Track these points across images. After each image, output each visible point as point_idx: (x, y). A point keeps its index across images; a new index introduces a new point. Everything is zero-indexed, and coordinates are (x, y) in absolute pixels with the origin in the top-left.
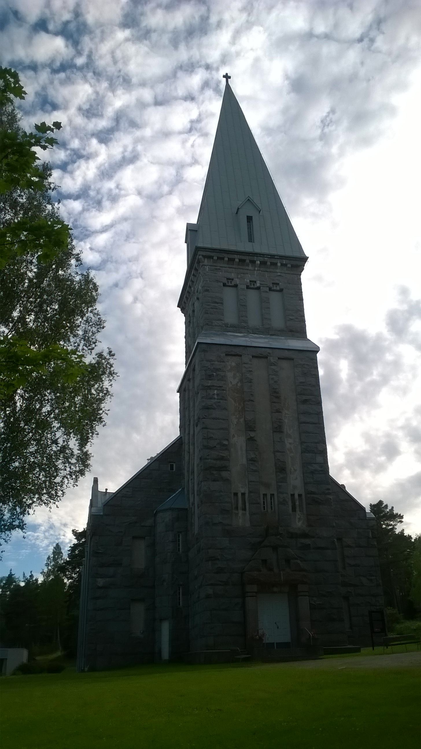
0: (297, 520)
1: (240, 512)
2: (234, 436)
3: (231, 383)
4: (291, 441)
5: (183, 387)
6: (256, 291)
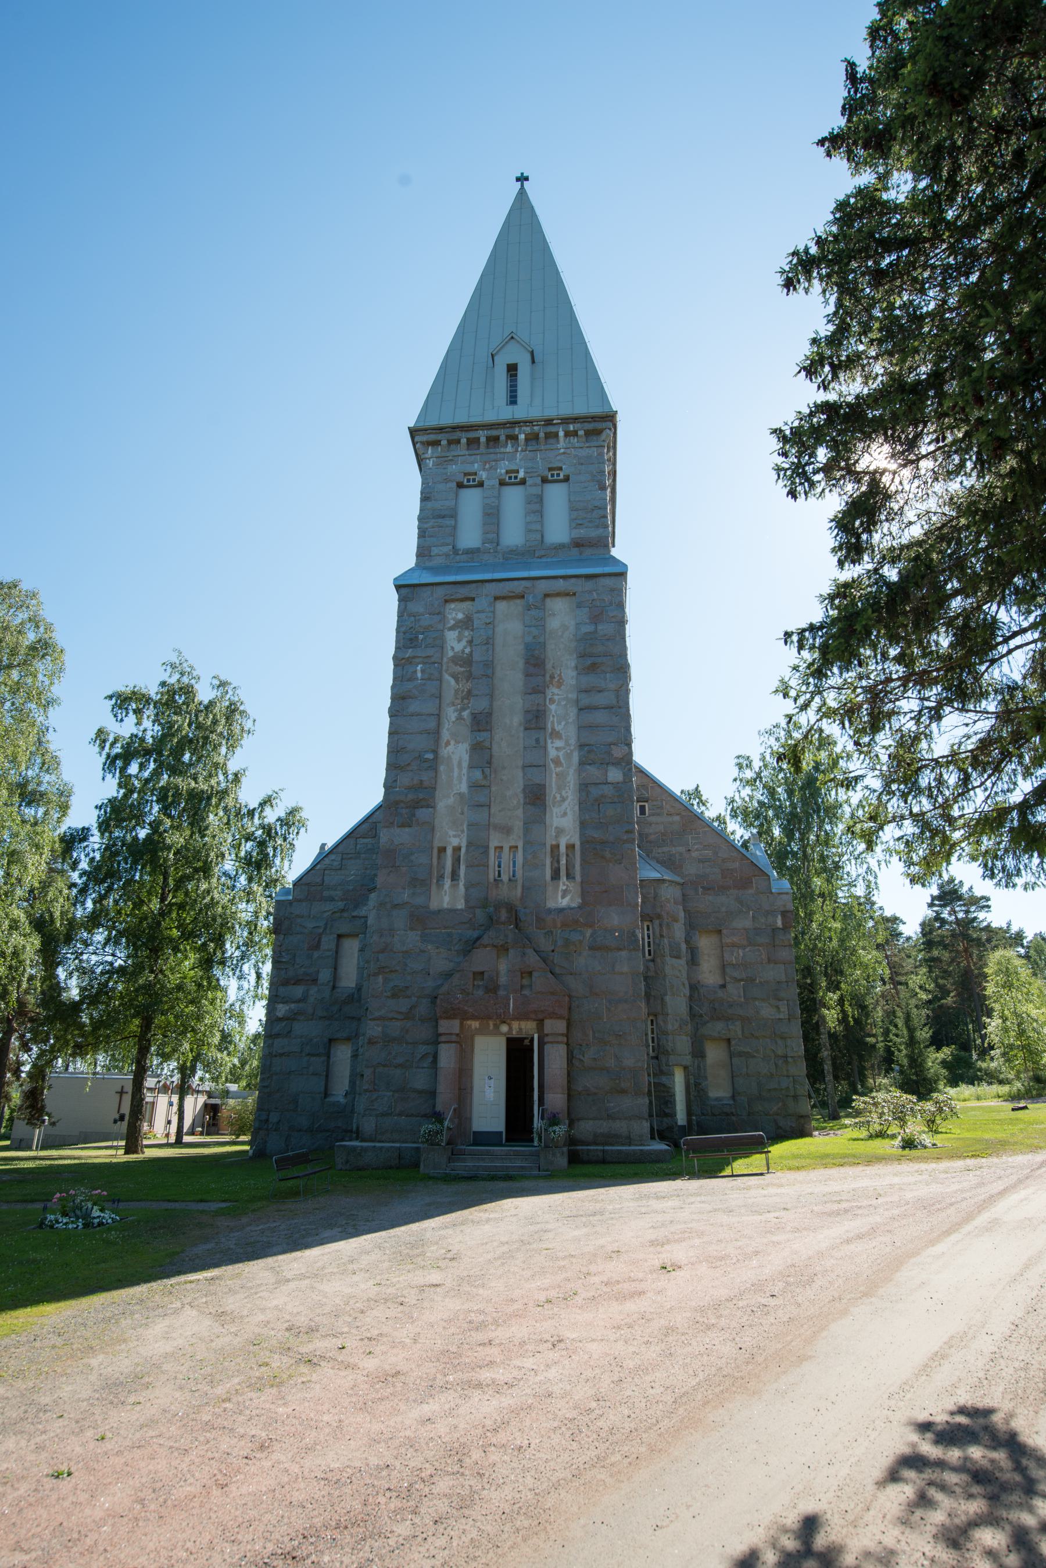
0: (560, 894)
1: (447, 883)
2: (448, 743)
3: (453, 648)
4: (559, 743)
5: (340, 849)
6: (519, 489)
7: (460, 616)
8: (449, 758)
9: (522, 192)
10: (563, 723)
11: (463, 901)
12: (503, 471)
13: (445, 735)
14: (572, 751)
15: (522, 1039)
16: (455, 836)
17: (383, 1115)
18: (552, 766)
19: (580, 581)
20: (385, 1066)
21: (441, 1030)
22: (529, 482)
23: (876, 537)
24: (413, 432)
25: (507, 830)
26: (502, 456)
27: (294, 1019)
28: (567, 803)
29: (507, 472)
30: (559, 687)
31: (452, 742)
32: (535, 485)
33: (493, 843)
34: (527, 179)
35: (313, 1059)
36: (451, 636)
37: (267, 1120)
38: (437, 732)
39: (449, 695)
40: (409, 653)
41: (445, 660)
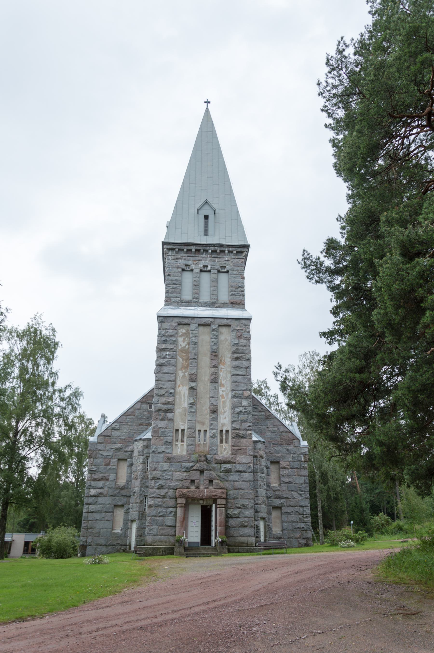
2: (179, 386)
3: (181, 345)
4: (223, 389)
7: (184, 331)
8: (180, 392)
9: (207, 111)
10: (225, 381)
11: (185, 451)
12: (202, 266)
13: (178, 382)
14: (228, 392)
15: (207, 506)
16: (182, 425)
17: (154, 535)
18: (221, 398)
19: (233, 321)
20: (155, 516)
21: (178, 502)
22: (213, 271)
23: (425, 79)
24: (164, 244)
25: (203, 424)
26: (201, 258)
27: (98, 496)
28: (226, 413)
29: (203, 266)
30: (223, 365)
31: (181, 386)
32: (214, 273)
33: (198, 428)
34: (209, 103)
35: (107, 514)
36: (180, 339)
37: (86, 541)
38: (175, 381)
39: (179, 366)
40: (164, 346)
41: (178, 350)
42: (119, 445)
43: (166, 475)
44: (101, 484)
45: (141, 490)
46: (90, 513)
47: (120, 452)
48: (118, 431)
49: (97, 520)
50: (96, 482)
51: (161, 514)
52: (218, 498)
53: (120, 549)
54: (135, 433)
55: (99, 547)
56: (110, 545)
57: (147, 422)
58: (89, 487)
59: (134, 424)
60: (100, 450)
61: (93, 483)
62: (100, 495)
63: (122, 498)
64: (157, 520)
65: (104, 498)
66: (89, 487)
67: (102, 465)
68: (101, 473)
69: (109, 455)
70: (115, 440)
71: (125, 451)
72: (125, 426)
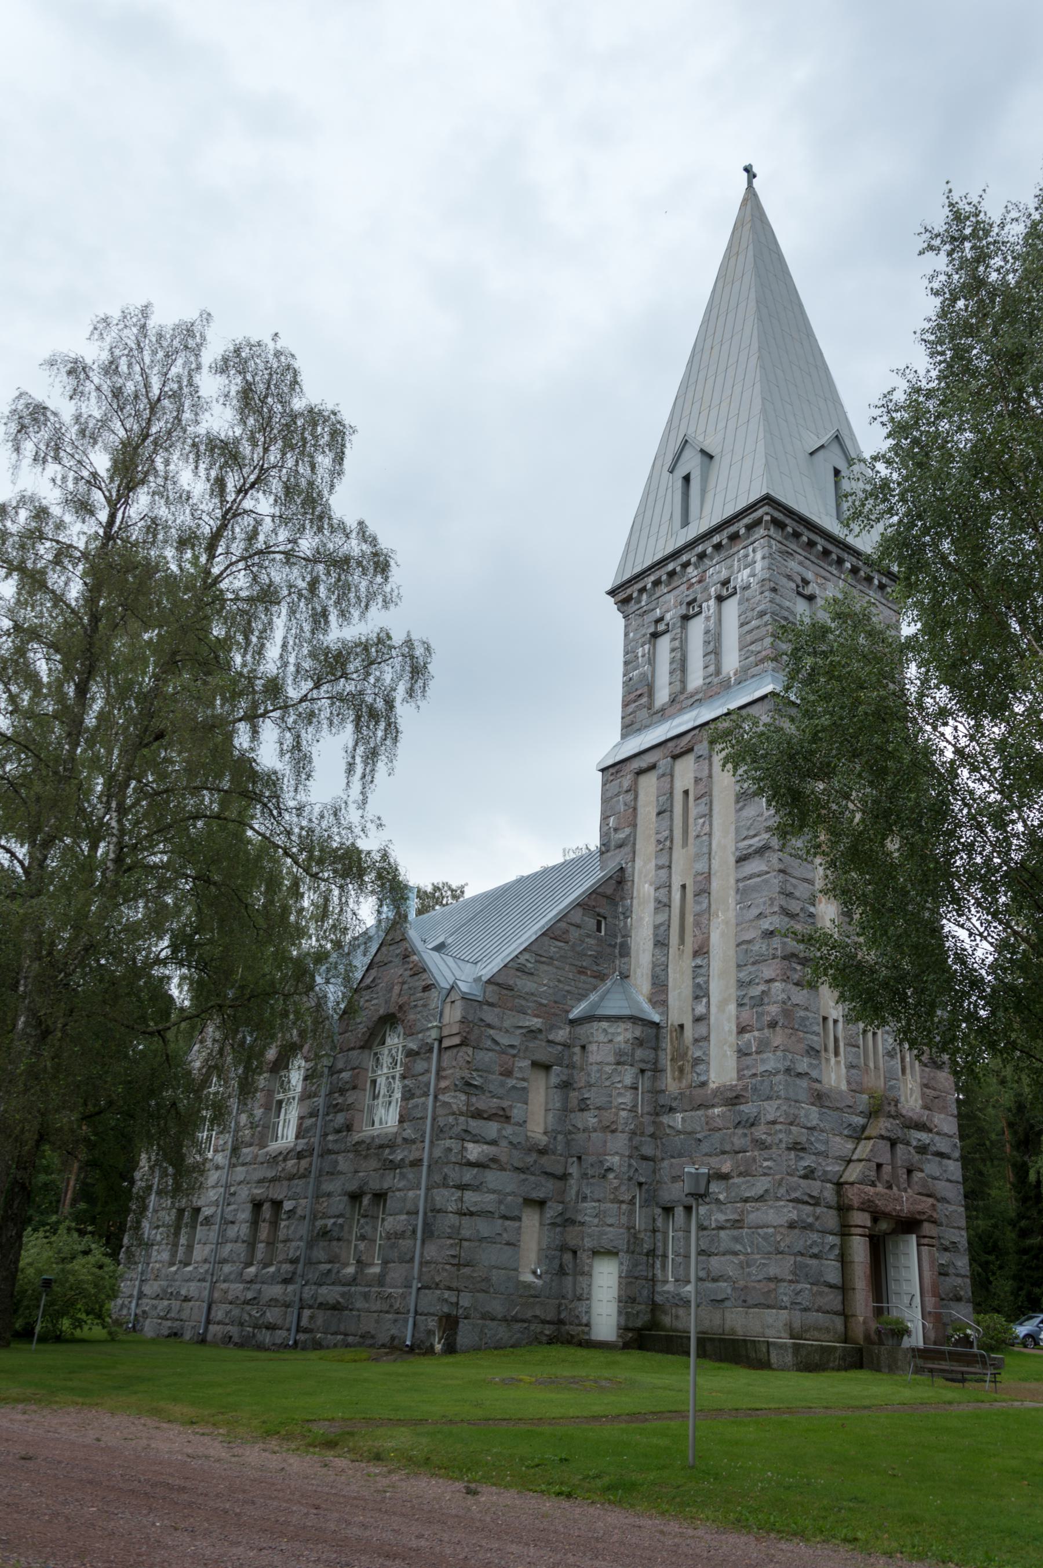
35: (508, 1223)
42: (536, 1020)
43: (818, 1140)
44: (492, 1129)
45: (630, 1165)
46: (465, 1214)
47: (537, 1042)
48: (531, 978)
49: (482, 1240)
50: (481, 1123)
51: (815, 1250)
52: (925, 1220)
53: (542, 1333)
54: (568, 991)
55: (488, 1322)
56: (516, 1320)
57: (595, 968)
58: (464, 1135)
59: (567, 967)
60: (489, 1026)
61: (474, 1125)
62: (492, 1165)
63: (542, 1179)
64: (807, 1266)
65: (499, 1173)
66: (464, 1135)
67: (493, 1073)
68: (493, 1097)
69: (512, 1046)
70: (523, 1003)
71: (549, 1041)
72: (545, 967)
